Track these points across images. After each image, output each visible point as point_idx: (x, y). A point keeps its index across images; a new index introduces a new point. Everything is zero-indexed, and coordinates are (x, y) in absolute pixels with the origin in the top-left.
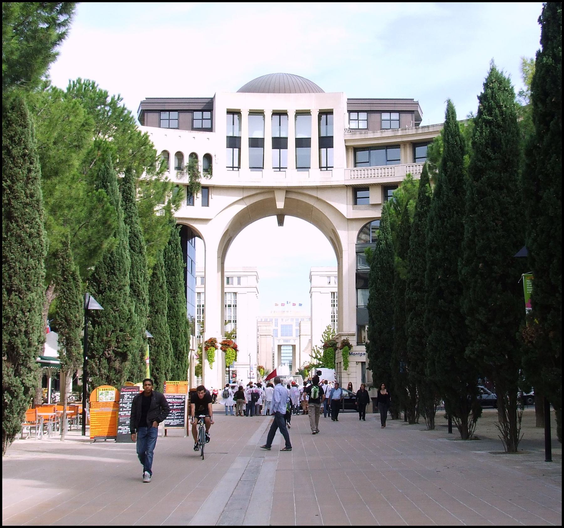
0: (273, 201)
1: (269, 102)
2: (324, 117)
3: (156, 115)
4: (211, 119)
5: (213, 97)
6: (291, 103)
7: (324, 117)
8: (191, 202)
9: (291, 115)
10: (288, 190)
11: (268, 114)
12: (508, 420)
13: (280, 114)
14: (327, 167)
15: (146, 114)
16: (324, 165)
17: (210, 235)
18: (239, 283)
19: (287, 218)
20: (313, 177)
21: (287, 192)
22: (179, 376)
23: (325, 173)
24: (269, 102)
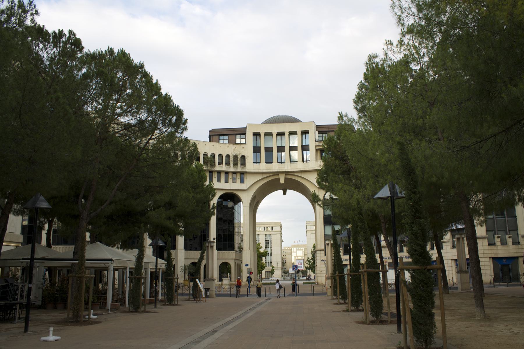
0: (278, 179)
1: (275, 129)
2: (304, 135)
3: (217, 137)
4: (245, 138)
6: (286, 128)
7: (304, 135)
8: (219, 181)
9: (262, 135)
10: (286, 173)
11: (275, 135)
12: (213, 221)
13: (281, 134)
14: (306, 161)
16: (305, 160)
17: (246, 199)
18: (272, 229)
19: (288, 191)
20: (299, 166)
23: (281, 165)
24: (275, 129)
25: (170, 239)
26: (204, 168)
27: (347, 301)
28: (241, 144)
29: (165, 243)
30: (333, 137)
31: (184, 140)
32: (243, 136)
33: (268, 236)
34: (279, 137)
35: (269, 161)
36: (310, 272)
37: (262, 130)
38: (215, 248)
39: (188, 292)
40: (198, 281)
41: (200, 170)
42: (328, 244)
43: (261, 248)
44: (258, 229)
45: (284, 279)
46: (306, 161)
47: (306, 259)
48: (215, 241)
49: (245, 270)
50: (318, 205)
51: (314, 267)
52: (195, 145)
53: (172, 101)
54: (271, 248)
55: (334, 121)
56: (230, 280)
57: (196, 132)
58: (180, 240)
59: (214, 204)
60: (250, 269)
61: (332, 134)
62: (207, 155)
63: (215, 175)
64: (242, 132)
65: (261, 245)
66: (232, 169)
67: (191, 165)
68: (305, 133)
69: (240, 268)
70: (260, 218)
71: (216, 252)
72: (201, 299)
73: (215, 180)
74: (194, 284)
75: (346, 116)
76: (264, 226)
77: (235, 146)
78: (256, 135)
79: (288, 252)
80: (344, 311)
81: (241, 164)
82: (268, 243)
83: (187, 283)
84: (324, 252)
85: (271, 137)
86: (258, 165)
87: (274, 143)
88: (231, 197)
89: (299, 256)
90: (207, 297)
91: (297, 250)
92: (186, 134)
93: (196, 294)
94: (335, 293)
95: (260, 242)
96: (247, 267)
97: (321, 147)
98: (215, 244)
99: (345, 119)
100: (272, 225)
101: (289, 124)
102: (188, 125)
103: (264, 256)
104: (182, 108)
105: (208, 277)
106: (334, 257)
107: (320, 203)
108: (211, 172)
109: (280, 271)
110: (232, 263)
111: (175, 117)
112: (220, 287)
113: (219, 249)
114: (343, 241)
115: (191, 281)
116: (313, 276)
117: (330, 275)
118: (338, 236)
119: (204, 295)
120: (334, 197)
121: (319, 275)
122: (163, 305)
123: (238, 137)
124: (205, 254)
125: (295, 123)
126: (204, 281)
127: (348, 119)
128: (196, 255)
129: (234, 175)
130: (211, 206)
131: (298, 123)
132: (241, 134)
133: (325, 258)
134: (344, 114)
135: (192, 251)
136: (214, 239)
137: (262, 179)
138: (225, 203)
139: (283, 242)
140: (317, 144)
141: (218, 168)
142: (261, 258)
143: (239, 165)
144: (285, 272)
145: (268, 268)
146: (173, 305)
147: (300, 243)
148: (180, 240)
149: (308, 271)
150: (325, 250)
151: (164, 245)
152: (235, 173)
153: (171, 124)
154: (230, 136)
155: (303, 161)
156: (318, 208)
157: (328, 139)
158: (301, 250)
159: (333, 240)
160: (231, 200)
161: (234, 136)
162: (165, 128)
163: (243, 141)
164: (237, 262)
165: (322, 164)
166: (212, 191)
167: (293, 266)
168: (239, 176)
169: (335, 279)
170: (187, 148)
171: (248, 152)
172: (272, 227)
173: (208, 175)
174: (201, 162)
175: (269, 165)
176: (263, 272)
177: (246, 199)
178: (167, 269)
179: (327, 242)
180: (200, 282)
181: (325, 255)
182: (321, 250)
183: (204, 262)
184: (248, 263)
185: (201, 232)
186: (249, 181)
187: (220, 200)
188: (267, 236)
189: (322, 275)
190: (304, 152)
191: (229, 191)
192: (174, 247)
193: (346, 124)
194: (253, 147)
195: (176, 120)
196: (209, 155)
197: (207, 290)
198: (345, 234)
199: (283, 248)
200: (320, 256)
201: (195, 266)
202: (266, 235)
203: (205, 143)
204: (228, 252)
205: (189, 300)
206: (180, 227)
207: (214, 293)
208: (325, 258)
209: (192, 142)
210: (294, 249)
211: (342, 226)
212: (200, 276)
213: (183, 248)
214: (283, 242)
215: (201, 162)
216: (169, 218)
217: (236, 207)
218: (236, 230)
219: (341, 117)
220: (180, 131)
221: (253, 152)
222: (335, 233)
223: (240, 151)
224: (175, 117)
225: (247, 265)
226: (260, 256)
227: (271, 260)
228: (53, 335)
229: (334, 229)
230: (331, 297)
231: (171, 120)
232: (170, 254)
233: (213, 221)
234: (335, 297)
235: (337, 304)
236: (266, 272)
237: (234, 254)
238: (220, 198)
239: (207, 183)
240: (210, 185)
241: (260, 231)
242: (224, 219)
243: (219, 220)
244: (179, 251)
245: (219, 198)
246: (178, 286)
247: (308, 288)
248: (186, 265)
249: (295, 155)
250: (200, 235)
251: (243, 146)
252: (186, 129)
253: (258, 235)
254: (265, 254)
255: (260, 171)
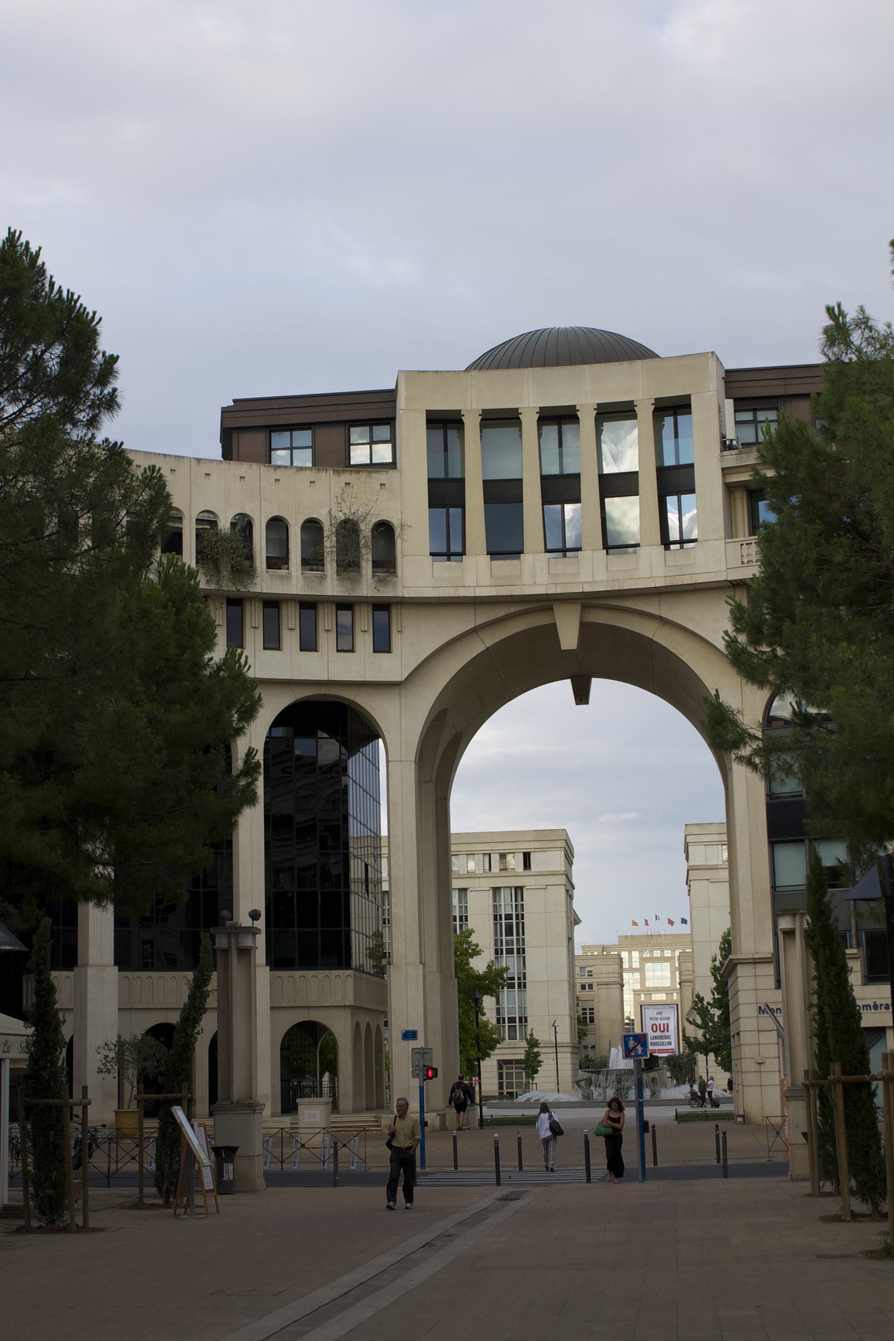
1: (530, 392)
3: (260, 437)
4: (392, 441)
5: (393, 387)
6: (584, 387)
7: (669, 421)
8: (273, 642)
10: (588, 601)
11: (529, 421)
12: (250, 829)
13: (558, 418)
14: (682, 542)
15: (235, 436)
16: (674, 535)
17: (401, 727)
18: (527, 864)
19: (599, 686)
20: (650, 568)
21: (584, 607)
22: (152, 964)
23: (561, 565)
24: (530, 392)
25: (47, 921)
26: (203, 585)
27: (885, 1207)
28: (372, 467)
29: (25, 937)
30: (802, 427)
31: (102, 455)
32: (383, 431)
33: (505, 898)
34: (551, 431)
35: (505, 545)
36: (707, 1066)
37: (472, 401)
38: (260, 955)
39: (134, 1167)
40: (179, 1113)
41: (180, 593)
42: (789, 934)
43: (476, 953)
44: (458, 865)
45: (588, 1097)
46: (682, 542)
47: (688, 1004)
48: (261, 924)
49: (401, 1055)
50: (740, 759)
51: (727, 1039)
52: (154, 481)
53: (42, 271)
54: (521, 951)
55: (808, 350)
56: (335, 1107)
57: (160, 414)
58: (98, 925)
59: (250, 753)
60: (422, 1053)
61: (801, 411)
62: (214, 523)
63: (254, 618)
64: (374, 411)
65: (473, 939)
66: (331, 586)
67: (137, 573)
68: (673, 408)
69: (379, 1050)
70: (467, 813)
71: (263, 974)
72: (198, 1200)
73: (254, 638)
74: (162, 1130)
75: (864, 322)
76: (487, 848)
77: (346, 477)
78: (445, 423)
79: (603, 971)
80: (871, 1254)
81: (376, 565)
82: (509, 932)
83: (130, 1123)
84: (770, 969)
85: (510, 432)
86: (453, 564)
87: (529, 460)
88: (333, 721)
89: (652, 989)
90: (223, 1187)
91: (643, 960)
92: (111, 429)
93: (172, 1176)
94: (826, 1167)
95: (471, 924)
96: (413, 1044)
97: (744, 477)
98: (261, 941)
99: (856, 337)
100: (527, 847)
101: (597, 367)
102: (123, 382)
103: (490, 991)
104: (89, 302)
105: (229, 1097)
106: (818, 978)
107: (746, 751)
108: (236, 603)
109: (566, 1060)
110: (341, 1028)
111: (57, 350)
112: (284, 1138)
113: (277, 961)
114: (859, 916)
115: (149, 1113)
116: (718, 1080)
117: (801, 1079)
118: (836, 896)
119: (208, 1182)
120: (812, 710)
121: (750, 1078)
122: (20, 1230)
123: (358, 434)
124: (213, 985)
125: (625, 365)
126: (211, 1114)
127: (870, 340)
128: (169, 990)
129: (382, 615)
130: (239, 764)
131: (638, 364)
132: (370, 423)
133: (775, 998)
134: (851, 313)
135: (155, 975)
136: (254, 915)
137: (475, 631)
138: (302, 747)
139: (577, 921)
140: (732, 459)
141: (266, 583)
142: (478, 1002)
143: (367, 567)
144: (590, 1064)
145: (512, 1049)
146: (66, 1230)
147: (663, 928)
148: (98, 925)
149: (700, 1057)
150: (775, 960)
151: (19, 947)
152: (345, 605)
153: (39, 383)
154: (321, 432)
155: (666, 542)
156: (739, 771)
157: (780, 436)
158: (662, 959)
159: (814, 916)
160: (333, 734)
161: (339, 431)
162: (14, 399)
163: (383, 453)
164: (364, 1019)
165: (753, 552)
166: (241, 693)
167: (626, 1039)
168: (364, 621)
169: (824, 1098)
170: (117, 494)
171: (406, 503)
172: (527, 857)
173: (219, 616)
174: (189, 556)
175: (505, 566)
176: (489, 1067)
177: (401, 727)
178: (34, 1060)
179: (785, 923)
180: (189, 1119)
181: (778, 985)
182: (756, 962)
183: (208, 1024)
184: (416, 1024)
185: (196, 882)
186: (415, 641)
187: (279, 732)
188: (505, 896)
189: (765, 1079)
190: (671, 501)
191: (323, 691)
192: (68, 956)
193: (865, 364)
194: (430, 481)
195: (64, 362)
196: (224, 524)
197: (224, 1154)
198: (869, 883)
199: (578, 952)
200: (753, 989)
201: (168, 1044)
202: (496, 890)
203: (205, 468)
204: (321, 974)
205: (139, 1205)
206: (92, 860)
207: (259, 1168)
208: (775, 998)
209: (140, 465)
210: (631, 958)
211: (853, 851)
212: (191, 1090)
213: (110, 958)
214: (577, 921)
215: (189, 556)
216: (43, 824)
217: (355, 764)
218: (356, 870)
219: (838, 330)
220: (82, 416)
221: (432, 505)
222: (823, 879)
223: (370, 502)
224: (57, 350)
225: (410, 1035)
226: (472, 989)
227: (523, 1008)
228: (340, 892)
229: (818, 860)
230: (807, 1186)
231: (38, 360)
232: (46, 992)
233: (250, 829)
234: (828, 1187)
235: (836, 1219)
236: (501, 1064)
237: (350, 983)
238: (279, 721)
239: (218, 654)
240: (232, 662)
241: (470, 875)
242: (299, 818)
243: (275, 824)
244: (90, 971)
245: (276, 723)
246: (89, 1143)
247: (700, 1145)
248: (127, 1037)
249: (628, 514)
250: (185, 896)
251: (382, 477)
252: (110, 403)
253: (463, 891)
254: (494, 982)
255: (463, 593)
